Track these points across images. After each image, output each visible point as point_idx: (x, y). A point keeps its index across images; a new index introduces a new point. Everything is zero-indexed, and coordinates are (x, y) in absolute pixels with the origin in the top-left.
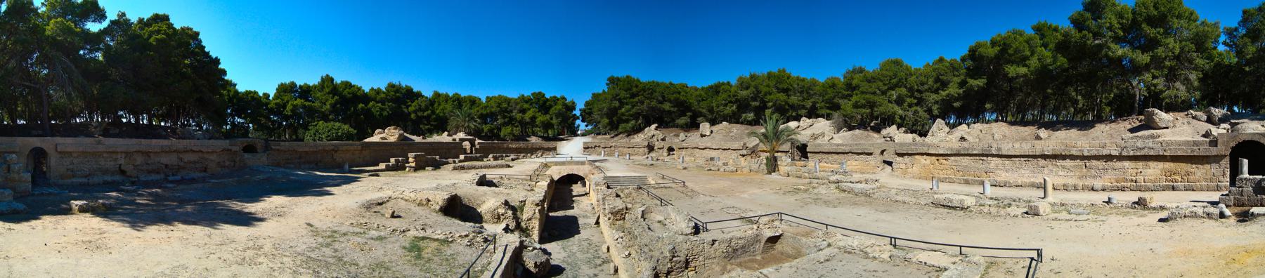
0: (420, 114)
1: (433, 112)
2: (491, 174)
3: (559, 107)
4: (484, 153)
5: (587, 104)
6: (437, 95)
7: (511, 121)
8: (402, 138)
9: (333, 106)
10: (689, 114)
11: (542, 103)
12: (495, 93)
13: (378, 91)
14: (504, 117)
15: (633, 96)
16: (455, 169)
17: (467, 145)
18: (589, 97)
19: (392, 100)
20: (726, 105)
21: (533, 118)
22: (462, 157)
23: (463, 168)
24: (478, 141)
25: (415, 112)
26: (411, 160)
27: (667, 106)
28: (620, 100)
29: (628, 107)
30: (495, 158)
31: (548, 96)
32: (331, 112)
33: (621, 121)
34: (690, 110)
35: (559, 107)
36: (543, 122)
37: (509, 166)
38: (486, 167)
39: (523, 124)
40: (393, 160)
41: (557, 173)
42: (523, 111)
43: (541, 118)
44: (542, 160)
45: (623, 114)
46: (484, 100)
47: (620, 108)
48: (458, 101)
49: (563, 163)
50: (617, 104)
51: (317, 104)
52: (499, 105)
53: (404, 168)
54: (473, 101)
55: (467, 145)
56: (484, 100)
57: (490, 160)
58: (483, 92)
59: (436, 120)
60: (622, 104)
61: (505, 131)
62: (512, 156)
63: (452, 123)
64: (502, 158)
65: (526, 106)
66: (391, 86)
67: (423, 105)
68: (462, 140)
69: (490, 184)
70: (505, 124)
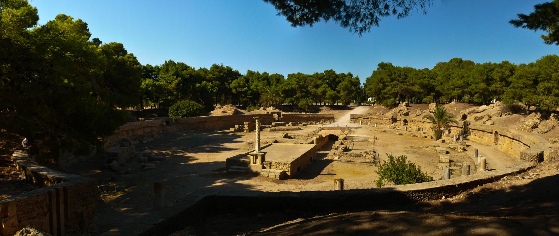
0: (239, 90)
1: (249, 89)
2: (290, 133)
3: (345, 83)
4: (287, 120)
5: (368, 80)
6: (251, 73)
7: (307, 94)
8: (236, 112)
9: (178, 85)
10: (432, 94)
11: (332, 79)
12: (295, 71)
13: (205, 71)
14: (302, 92)
15: (393, 80)
16: (271, 131)
17: (276, 116)
18: (370, 75)
19: (217, 79)
20: (454, 89)
21: (324, 92)
22: (273, 124)
23: (275, 130)
24: (283, 113)
25: (235, 88)
26: (245, 126)
27: (416, 88)
28: (383, 83)
29: (390, 88)
30: (293, 125)
31: (338, 73)
32: (176, 89)
33: (385, 98)
34: (434, 91)
35: (345, 83)
36: (331, 96)
37: (300, 129)
38: (287, 130)
39: (316, 97)
40: (237, 126)
41: (324, 133)
42: (317, 86)
43: (330, 92)
44: (321, 126)
45: (385, 94)
46: (286, 78)
47: (384, 89)
48: (266, 78)
49: (281, 130)
50: (381, 86)
51: (163, 83)
52: (298, 83)
53: (243, 131)
54: (278, 78)
55: (276, 116)
56: (286, 78)
57: (290, 126)
58: (285, 69)
59: (251, 94)
60: (385, 86)
61: (302, 103)
62: (304, 123)
63: (264, 97)
64: (297, 124)
65: (319, 82)
66: (215, 67)
67: (242, 83)
68: (273, 113)
69: (290, 137)
70: (302, 97)
